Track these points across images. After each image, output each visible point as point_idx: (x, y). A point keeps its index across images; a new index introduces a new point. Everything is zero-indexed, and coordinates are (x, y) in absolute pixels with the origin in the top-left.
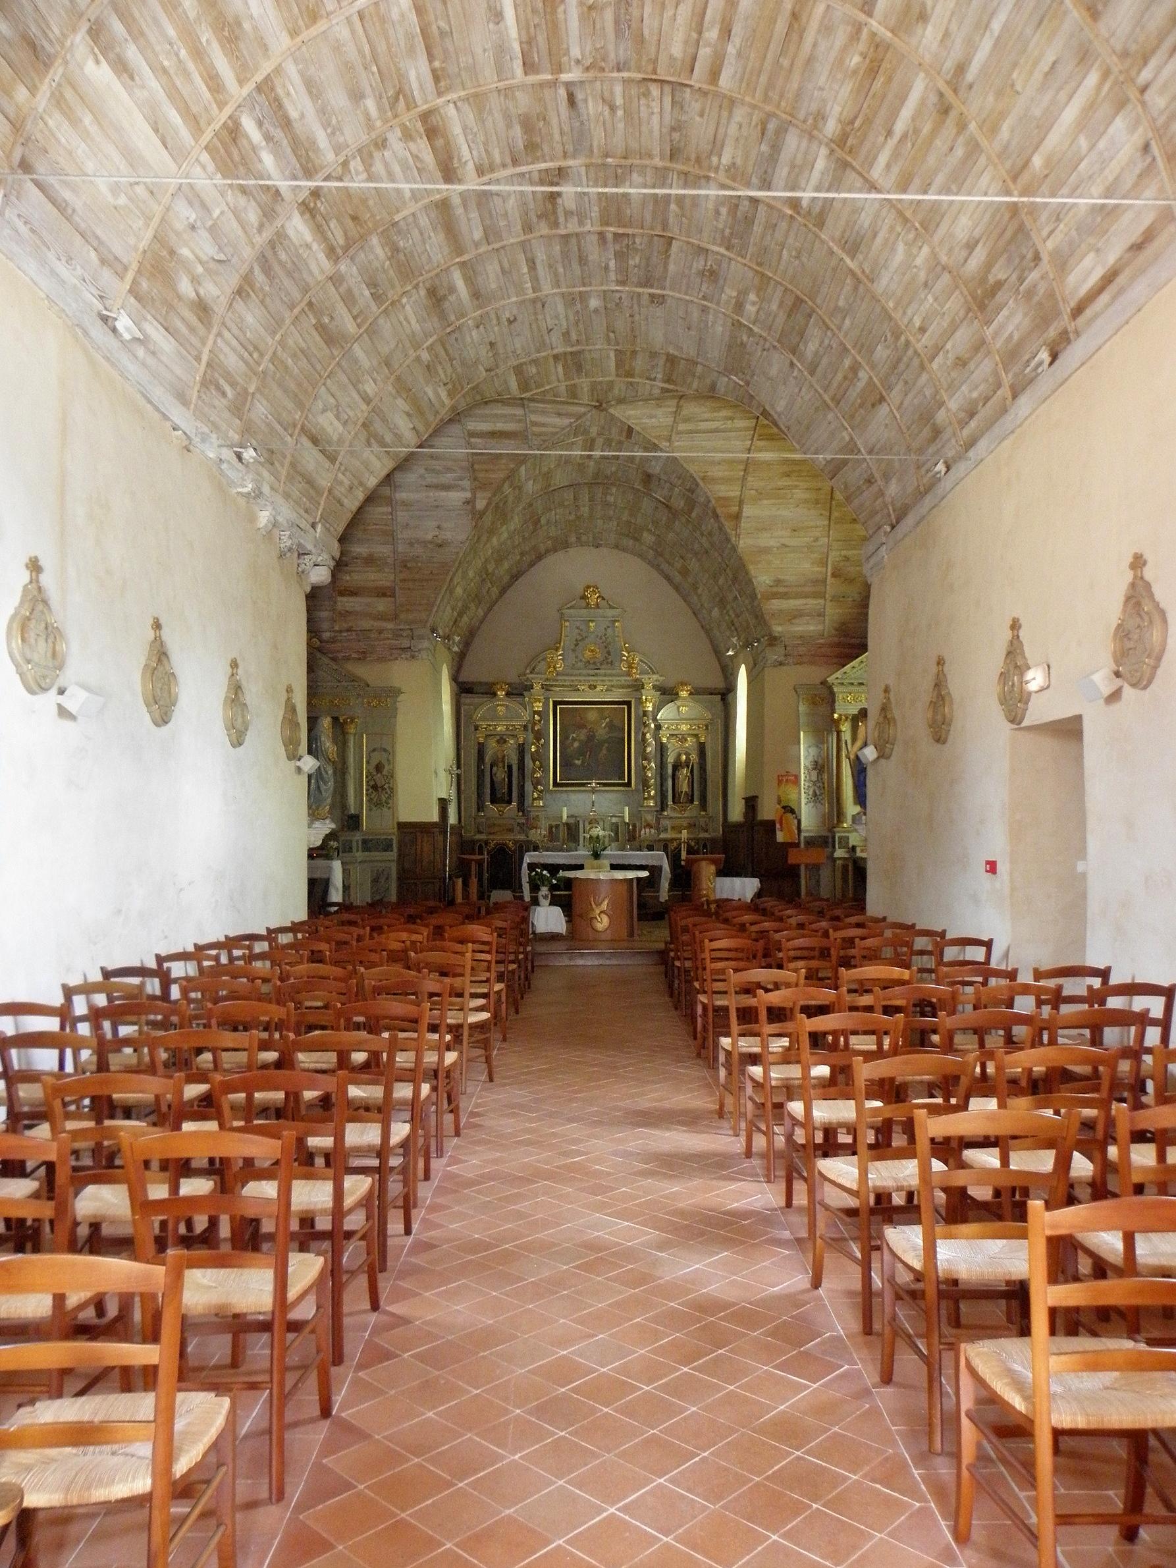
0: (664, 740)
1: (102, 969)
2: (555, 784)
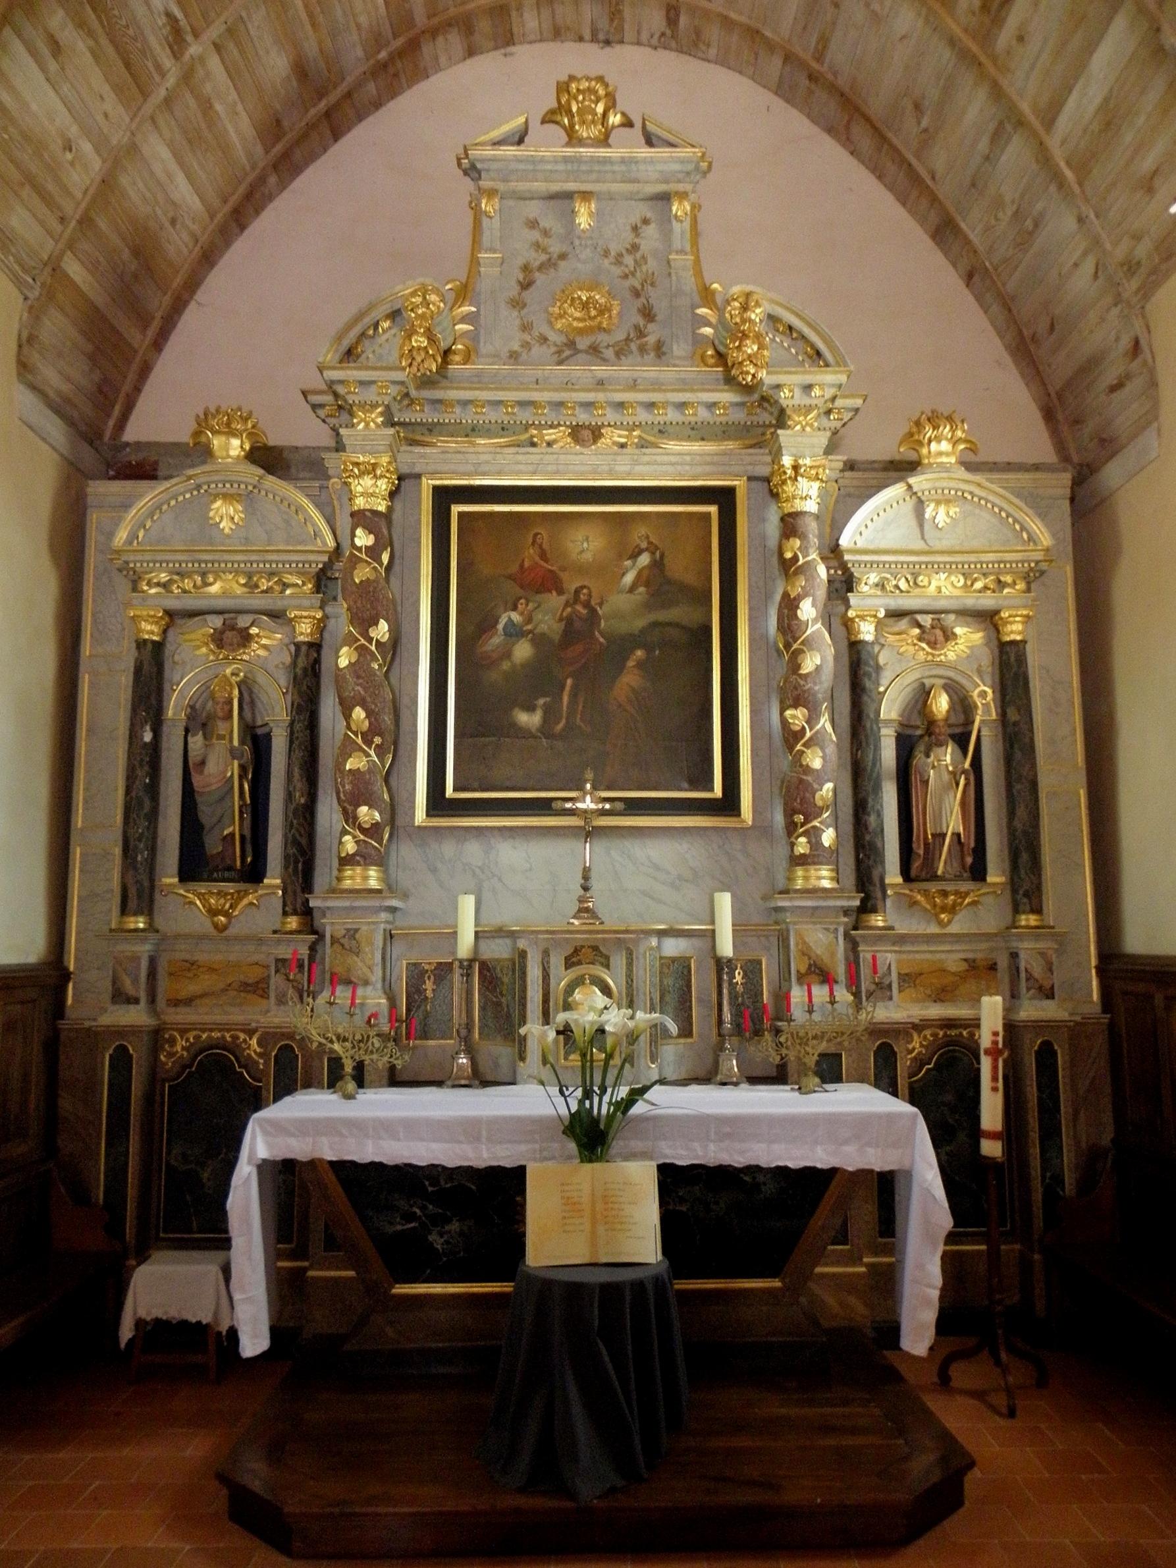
0: (867, 631)
1: (566, 969)
2: (438, 803)
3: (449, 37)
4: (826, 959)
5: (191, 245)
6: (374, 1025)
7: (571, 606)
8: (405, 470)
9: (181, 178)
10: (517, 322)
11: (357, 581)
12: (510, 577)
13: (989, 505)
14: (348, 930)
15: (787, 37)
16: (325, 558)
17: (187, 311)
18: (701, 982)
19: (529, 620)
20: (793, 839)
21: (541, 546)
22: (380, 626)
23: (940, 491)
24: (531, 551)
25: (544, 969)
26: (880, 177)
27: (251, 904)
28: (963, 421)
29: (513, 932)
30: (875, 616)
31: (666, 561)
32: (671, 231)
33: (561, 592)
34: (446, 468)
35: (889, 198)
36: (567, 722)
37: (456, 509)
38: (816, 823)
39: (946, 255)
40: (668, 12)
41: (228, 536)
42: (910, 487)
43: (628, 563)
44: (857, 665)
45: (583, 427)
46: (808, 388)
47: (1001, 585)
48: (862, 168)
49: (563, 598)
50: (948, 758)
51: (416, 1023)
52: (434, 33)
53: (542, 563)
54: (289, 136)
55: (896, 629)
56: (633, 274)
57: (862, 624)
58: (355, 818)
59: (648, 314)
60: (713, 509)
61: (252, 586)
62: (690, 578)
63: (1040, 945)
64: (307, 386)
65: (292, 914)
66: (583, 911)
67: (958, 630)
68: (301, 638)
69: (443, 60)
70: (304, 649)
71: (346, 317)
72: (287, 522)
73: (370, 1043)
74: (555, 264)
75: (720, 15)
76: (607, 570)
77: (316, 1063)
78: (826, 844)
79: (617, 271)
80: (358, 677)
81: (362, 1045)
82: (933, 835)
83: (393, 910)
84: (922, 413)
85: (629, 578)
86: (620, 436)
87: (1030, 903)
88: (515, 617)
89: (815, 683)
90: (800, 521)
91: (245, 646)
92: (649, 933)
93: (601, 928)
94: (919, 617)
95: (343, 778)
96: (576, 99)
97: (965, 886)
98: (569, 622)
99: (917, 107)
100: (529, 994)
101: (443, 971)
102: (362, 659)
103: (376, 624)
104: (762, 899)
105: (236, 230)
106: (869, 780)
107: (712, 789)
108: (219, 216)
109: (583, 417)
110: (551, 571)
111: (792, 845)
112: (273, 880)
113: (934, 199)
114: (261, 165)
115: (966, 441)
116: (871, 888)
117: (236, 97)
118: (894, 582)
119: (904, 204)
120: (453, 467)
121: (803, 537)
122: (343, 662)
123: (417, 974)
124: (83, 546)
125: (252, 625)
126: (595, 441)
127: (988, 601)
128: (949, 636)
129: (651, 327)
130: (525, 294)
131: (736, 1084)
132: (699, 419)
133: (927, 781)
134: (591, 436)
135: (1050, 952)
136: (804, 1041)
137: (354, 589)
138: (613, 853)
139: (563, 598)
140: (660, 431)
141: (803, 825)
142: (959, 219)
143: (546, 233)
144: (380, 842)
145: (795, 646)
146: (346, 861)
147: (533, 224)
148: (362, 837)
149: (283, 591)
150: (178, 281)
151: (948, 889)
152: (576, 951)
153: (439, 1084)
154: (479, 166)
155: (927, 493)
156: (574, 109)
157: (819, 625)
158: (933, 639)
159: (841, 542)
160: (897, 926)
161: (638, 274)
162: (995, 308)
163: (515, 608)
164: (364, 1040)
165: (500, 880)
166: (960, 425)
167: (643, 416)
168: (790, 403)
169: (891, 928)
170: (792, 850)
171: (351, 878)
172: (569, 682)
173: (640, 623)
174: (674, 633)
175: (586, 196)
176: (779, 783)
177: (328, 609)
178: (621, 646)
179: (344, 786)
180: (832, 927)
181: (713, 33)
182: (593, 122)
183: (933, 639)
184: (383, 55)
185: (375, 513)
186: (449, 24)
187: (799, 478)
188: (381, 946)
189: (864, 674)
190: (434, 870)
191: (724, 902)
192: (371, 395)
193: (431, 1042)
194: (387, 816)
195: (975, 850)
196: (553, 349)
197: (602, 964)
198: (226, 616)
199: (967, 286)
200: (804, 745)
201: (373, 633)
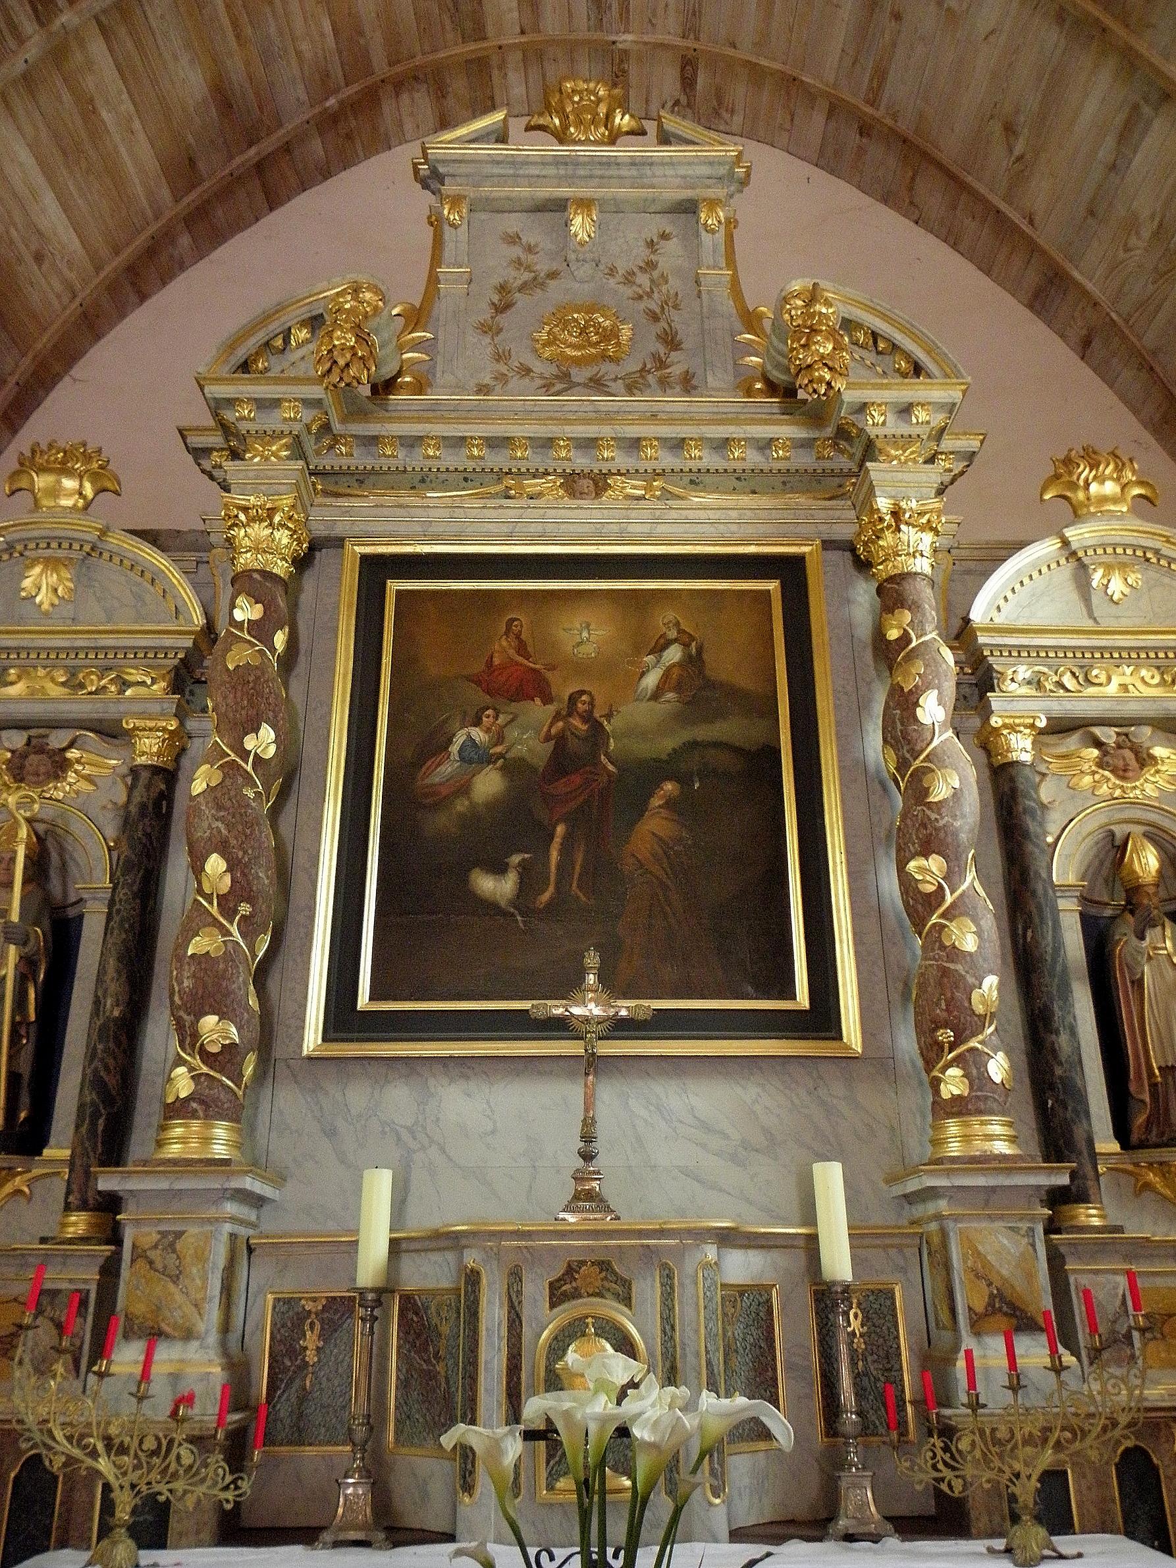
0: (1021, 747)
1: (553, 1306)
2: (343, 1018)
3: (417, 95)
4: (1019, 1285)
5: (66, 300)
6: (184, 1420)
7: (564, 718)
8: (320, 531)
9: (49, 199)
10: (490, 350)
11: (231, 667)
12: (469, 679)
14: (164, 1234)
15: (832, 81)
16: (189, 643)
17: (60, 386)
18: (793, 1334)
19: (500, 739)
20: (936, 1073)
21: (518, 637)
22: (262, 732)
23: (1110, 550)
24: (504, 643)
25: (512, 1307)
26: (954, 246)
27: (18, 1192)
28: (1131, 460)
29: (457, 1235)
30: (1032, 726)
31: (705, 656)
32: (700, 245)
33: (547, 699)
34: (379, 528)
35: (970, 268)
36: (557, 888)
37: (394, 586)
38: (973, 1043)
39: (1049, 325)
40: (683, 69)
41: (46, 614)
42: (1066, 543)
43: (650, 659)
44: (1009, 800)
45: (581, 475)
46: (906, 410)
48: (931, 237)
49: (551, 708)
50: (1169, 944)
51: (284, 1409)
52: (399, 85)
53: (520, 659)
54: (207, 184)
55: (1062, 750)
56: (649, 295)
57: (1013, 737)
58: (196, 1035)
59: (671, 341)
60: (773, 586)
61: (73, 684)
62: (744, 680)
64: (184, 424)
65: (79, 1209)
66: (586, 1197)
68: (141, 760)
69: (408, 126)
70: (145, 775)
71: (243, 319)
72: (139, 597)
73: (173, 1456)
74: (543, 284)
75: (747, 64)
76: (617, 670)
77: (80, 1496)
78: (997, 1079)
79: (629, 291)
80: (220, 807)
81: (156, 1460)
82: (1160, 1068)
83: (258, 1201)
84: (1070, 450)
85: (651, 680)
86: (635, 487)
88: (478, 734)
89: (954, 817)
90: (908, 586)
91: (57, 778)
92: (701, 1235)
93: (615, 1226)
94: (1097, 731)
95: (180, 969)
96: (571, 98)
98: (560, 741)
99: (1010, 129)
100: (484, 1354)
101: (337, 1311)
102: (228, 782)
103: (256, 730)
104: (887, 1182)
105: (133, 298)
106: (1052, 976)
107: (793, 997)
108: (108, 269)
109: (581, 462)
110: (534, 670)
111: (936, 1084)
112: (57, 1151)
113: (1033, 248)
114: (168, 214)
115: (1140, 483)
117: (132, 108)
118: (1055, 679)
119: (988, 273)
120: (390, 527)
121: (915, 607)
122: (198, 787)
123: (291, 1320)
125: (71, 745)
126: (598, 495)
128: (1145, 760)
129: (674, 356)
130: (503, 320)
131: (875, 1539)
132: (748, 465)
134: (592, 488)
136: (997, 1443)
137: (226, 678)
138: (631, 1102)
139: (551, 708)
140: (692, 482)
142: (1068, 266)
143: (530, 249)
144: (237, 1078)
146: (178, 1109)
147: (513, 239)
148: (205, 1069)
149: (121, 692)
150: (43, 342)
152: (571, 1271)
153: (307, 1535)
154: (441, 170)
155: (1090, 552)
156: (569, 109)
157: (950, 733)
158: (1121, 763)
159: (972, 616)
160: (1127, 1225)
161: (656, 295)
162: (1127, 375)
163: (477, 723)
164: (163, 1449)
165: (443, 1150)
166: (1128, 464)
167: (668, 461)
168: (880, 431)
169: (1119, 1229)
170: (937, 1092)
171: (183, 1140)
172: (560, 829)
173: (669, 744)
174: (724, 760)
175: (585, 204)
176: (900, 986)
177: (191, 724)
178: (643, 776)
179: (180, 983)
181: (739, 92)
182: (593, 122)
183: (1121, 763)
184: (332, 102)
185: (267, 575)
186: (414, 78)
187: (903, 527)
188: (221, 1262)
189: (1025, 811)
190: (331, 1133)
191: (830, 1180)
192: (273, 421)
193: (310, 1451)
194: (254, 1032)
196: (540, 382)
197: (617, 1296)
198: (33, 732)
199: (1082, 358)
200: (943, 916)
201: (250, 743)
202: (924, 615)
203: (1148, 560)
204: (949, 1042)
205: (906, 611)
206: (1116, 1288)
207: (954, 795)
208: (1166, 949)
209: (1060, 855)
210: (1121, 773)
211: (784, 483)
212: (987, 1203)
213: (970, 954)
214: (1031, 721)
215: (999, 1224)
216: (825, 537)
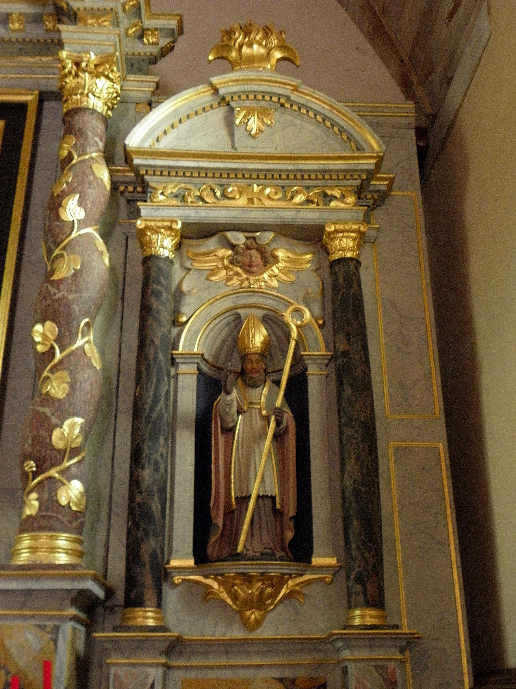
0: (164, 246)
13: (311, 114)
30: (170, 228)
38: (54, 473)
47: (327, 198)
63: (379, 654)
67: (281, 254)
82: (236, 498)
87: (365, 593)
97: (275, 569)
116: (137, 570)
121: (80, 134)
124: (458, 625)
127: (310, 216)
133: (232, 430)
135: (392, 665)
141: (35, 475)
145: (56, 252)
151: (253, 572)
180: (51, 624)
195: (296, 519)
202: (86, 139)
203: (282, 105)
204: (33, 472)
205: (72, 137)
206: (147, 677)
207: (74, 275)
208: (259, 404)
209: (189, 331)
210: (247, 268)
211: (21, 50)
212: (23, 606)
213: (59, 400)
214: (169, 224)
215: (30, 623)
216: (44, 89)
